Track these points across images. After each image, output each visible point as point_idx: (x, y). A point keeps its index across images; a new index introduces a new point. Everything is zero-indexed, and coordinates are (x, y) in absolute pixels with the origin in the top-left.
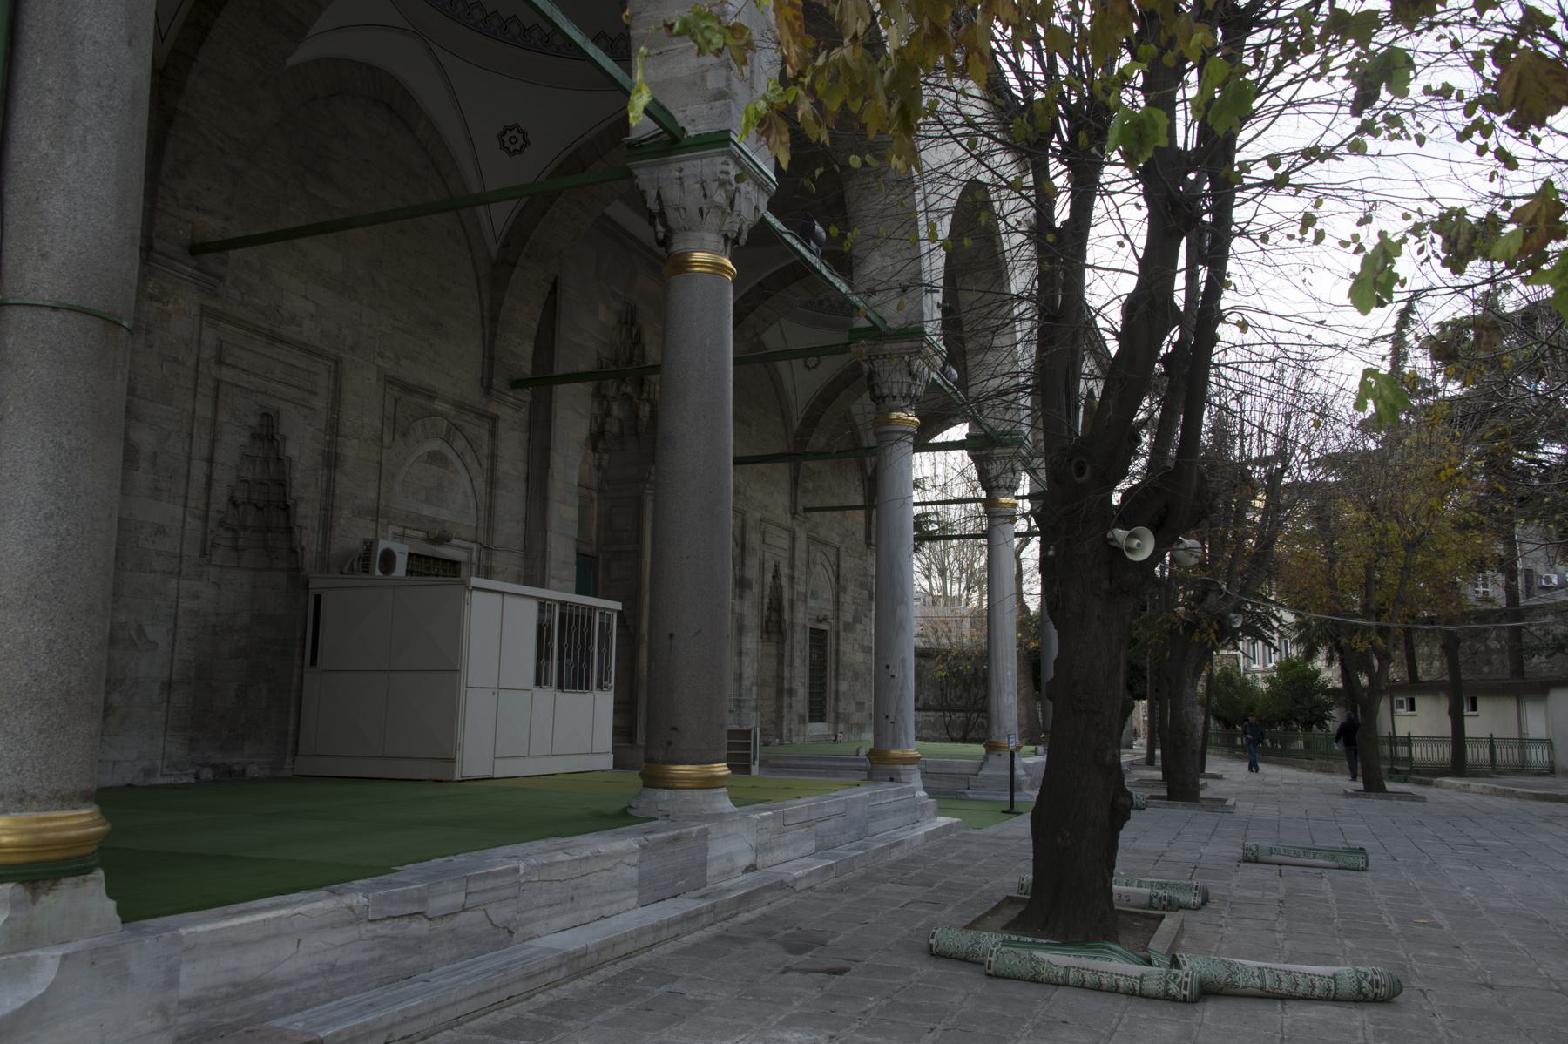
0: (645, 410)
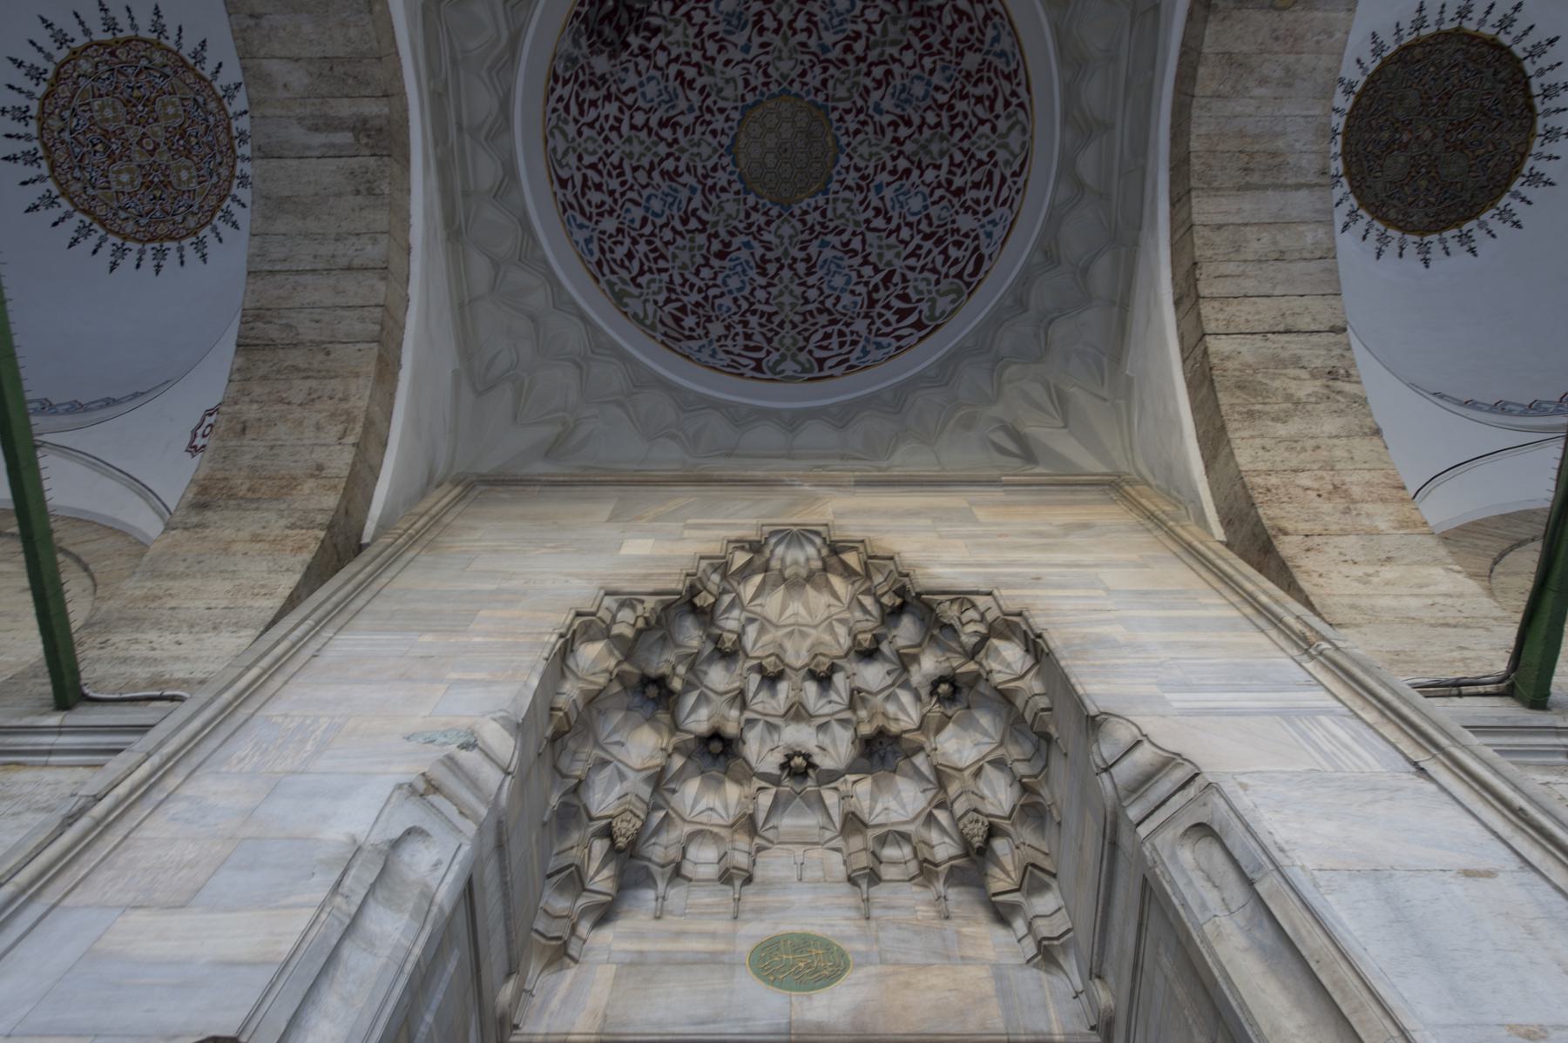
0: (1009, 658)
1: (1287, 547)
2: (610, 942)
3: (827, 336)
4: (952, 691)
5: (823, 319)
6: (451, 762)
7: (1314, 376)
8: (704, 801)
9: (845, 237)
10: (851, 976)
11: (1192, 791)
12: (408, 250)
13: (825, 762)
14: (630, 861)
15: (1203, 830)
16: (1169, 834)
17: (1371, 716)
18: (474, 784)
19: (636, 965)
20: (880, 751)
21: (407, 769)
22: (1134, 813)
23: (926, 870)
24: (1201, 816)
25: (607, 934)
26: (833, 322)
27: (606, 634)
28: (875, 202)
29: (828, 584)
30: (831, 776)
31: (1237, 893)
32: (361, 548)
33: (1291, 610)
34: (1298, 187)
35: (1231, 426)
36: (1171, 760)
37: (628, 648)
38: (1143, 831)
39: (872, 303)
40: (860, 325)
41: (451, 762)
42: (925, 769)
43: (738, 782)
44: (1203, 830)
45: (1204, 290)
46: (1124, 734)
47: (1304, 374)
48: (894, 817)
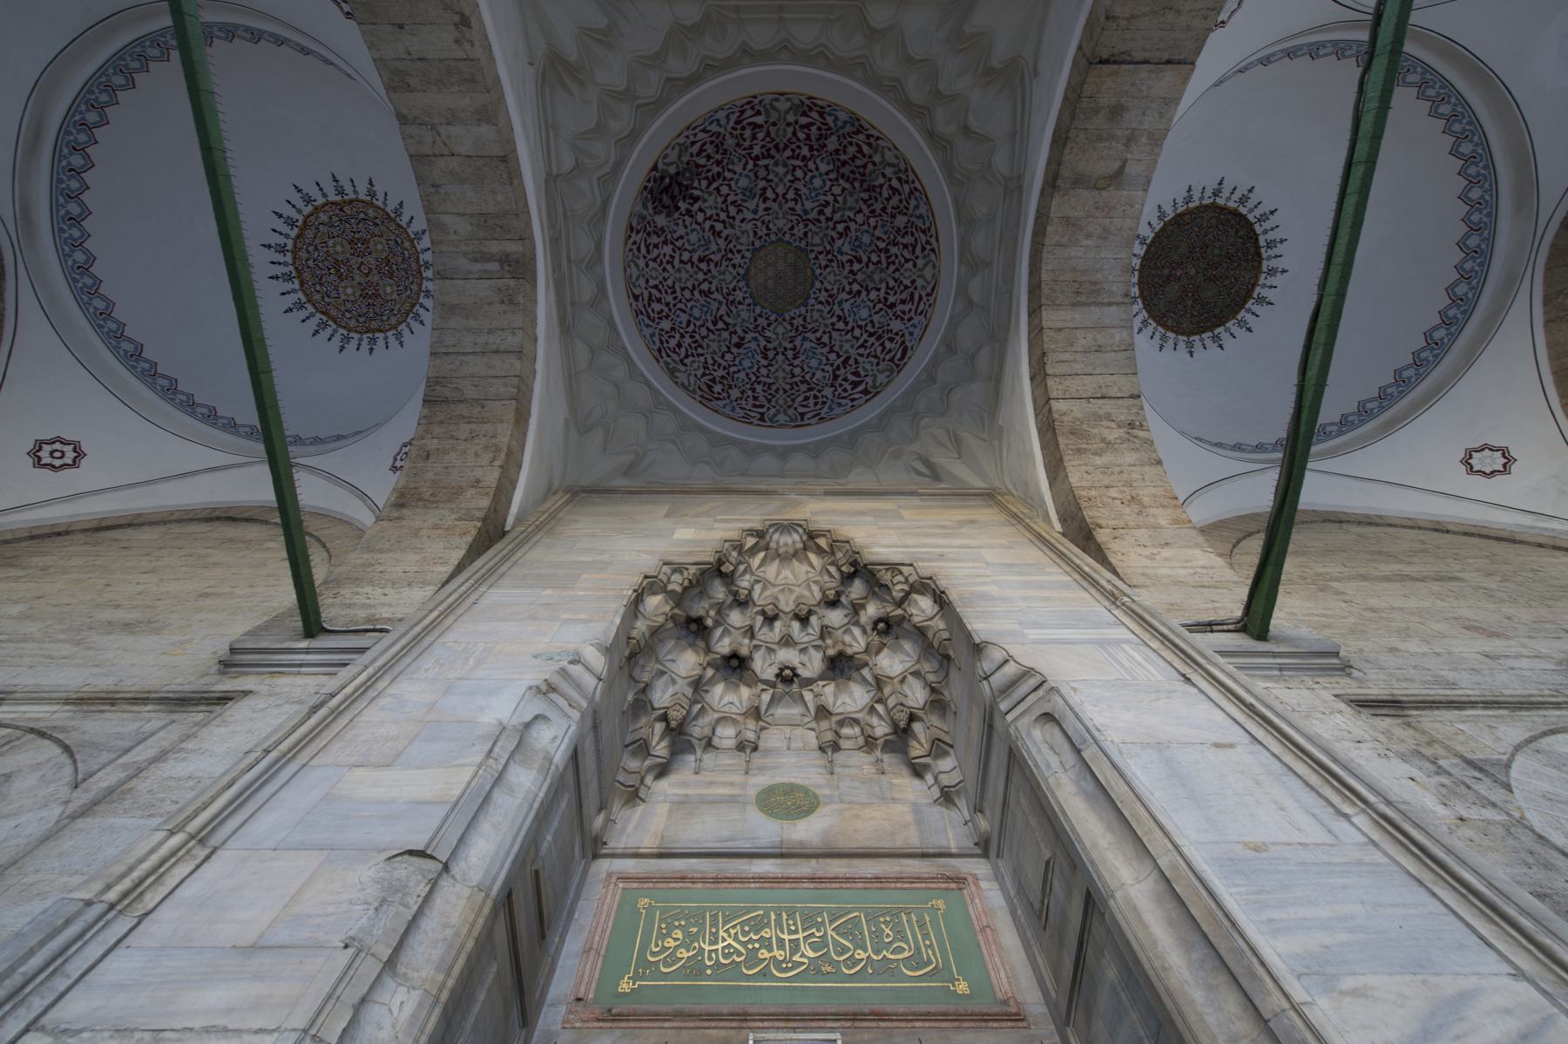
0: (923, 607)
1: (1102, 536)
2: (666, 788)
3: (807, 398)
4: (887, 628)
5: (804, 387)
6: (563, 672)
7: (1119, 427)
8: (726, 697)
9: (818, 335)
10: (821, 811)
11: (1041, 692)
12: (536, 340)
13: (805, 673)
14: (679, 737)
15: (1048, 717)
16: (1026, 720)
17: (1155, 644)
18: (578, 686)
19: (682, 805)
20: (840, 666)
21: (535, 677)
22: (1003, 706)
23: (869, 743)
24: (1047, 708)
25: (664, 784)
26: (811, 389)
27: (664, 590)
28: (838, 312)
29: (807, 559)
30: (808, 682)
31: (1069, 758)
32: (504, 534)
33: (1103, 577)
34: (1110, 304)
35: (1066, 458)
36: (1028, 672)
37: (678, 599)
38: (1009, 718)
39: (836, 377)
40: (828, 392)
41: (563, 672)
42: (869, 677)
43: (749, 686)
44: (1048, 717)
45: (1049, 371)
46: (998, 656)
47: (1113, 425)
48: (849, 709)
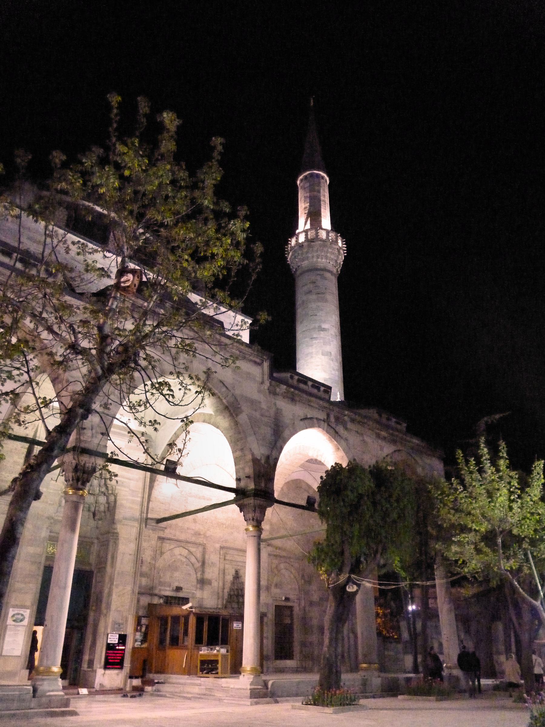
0: (112, 498)
